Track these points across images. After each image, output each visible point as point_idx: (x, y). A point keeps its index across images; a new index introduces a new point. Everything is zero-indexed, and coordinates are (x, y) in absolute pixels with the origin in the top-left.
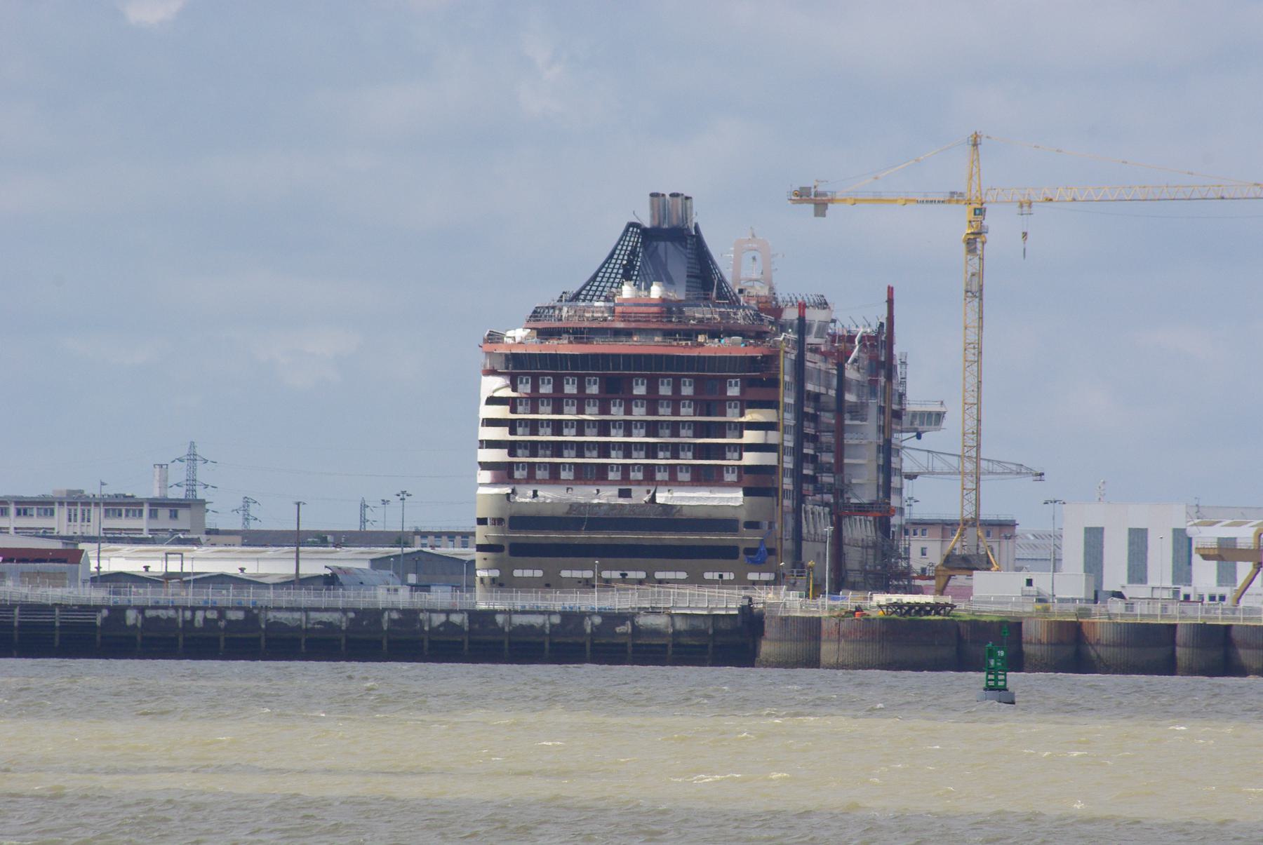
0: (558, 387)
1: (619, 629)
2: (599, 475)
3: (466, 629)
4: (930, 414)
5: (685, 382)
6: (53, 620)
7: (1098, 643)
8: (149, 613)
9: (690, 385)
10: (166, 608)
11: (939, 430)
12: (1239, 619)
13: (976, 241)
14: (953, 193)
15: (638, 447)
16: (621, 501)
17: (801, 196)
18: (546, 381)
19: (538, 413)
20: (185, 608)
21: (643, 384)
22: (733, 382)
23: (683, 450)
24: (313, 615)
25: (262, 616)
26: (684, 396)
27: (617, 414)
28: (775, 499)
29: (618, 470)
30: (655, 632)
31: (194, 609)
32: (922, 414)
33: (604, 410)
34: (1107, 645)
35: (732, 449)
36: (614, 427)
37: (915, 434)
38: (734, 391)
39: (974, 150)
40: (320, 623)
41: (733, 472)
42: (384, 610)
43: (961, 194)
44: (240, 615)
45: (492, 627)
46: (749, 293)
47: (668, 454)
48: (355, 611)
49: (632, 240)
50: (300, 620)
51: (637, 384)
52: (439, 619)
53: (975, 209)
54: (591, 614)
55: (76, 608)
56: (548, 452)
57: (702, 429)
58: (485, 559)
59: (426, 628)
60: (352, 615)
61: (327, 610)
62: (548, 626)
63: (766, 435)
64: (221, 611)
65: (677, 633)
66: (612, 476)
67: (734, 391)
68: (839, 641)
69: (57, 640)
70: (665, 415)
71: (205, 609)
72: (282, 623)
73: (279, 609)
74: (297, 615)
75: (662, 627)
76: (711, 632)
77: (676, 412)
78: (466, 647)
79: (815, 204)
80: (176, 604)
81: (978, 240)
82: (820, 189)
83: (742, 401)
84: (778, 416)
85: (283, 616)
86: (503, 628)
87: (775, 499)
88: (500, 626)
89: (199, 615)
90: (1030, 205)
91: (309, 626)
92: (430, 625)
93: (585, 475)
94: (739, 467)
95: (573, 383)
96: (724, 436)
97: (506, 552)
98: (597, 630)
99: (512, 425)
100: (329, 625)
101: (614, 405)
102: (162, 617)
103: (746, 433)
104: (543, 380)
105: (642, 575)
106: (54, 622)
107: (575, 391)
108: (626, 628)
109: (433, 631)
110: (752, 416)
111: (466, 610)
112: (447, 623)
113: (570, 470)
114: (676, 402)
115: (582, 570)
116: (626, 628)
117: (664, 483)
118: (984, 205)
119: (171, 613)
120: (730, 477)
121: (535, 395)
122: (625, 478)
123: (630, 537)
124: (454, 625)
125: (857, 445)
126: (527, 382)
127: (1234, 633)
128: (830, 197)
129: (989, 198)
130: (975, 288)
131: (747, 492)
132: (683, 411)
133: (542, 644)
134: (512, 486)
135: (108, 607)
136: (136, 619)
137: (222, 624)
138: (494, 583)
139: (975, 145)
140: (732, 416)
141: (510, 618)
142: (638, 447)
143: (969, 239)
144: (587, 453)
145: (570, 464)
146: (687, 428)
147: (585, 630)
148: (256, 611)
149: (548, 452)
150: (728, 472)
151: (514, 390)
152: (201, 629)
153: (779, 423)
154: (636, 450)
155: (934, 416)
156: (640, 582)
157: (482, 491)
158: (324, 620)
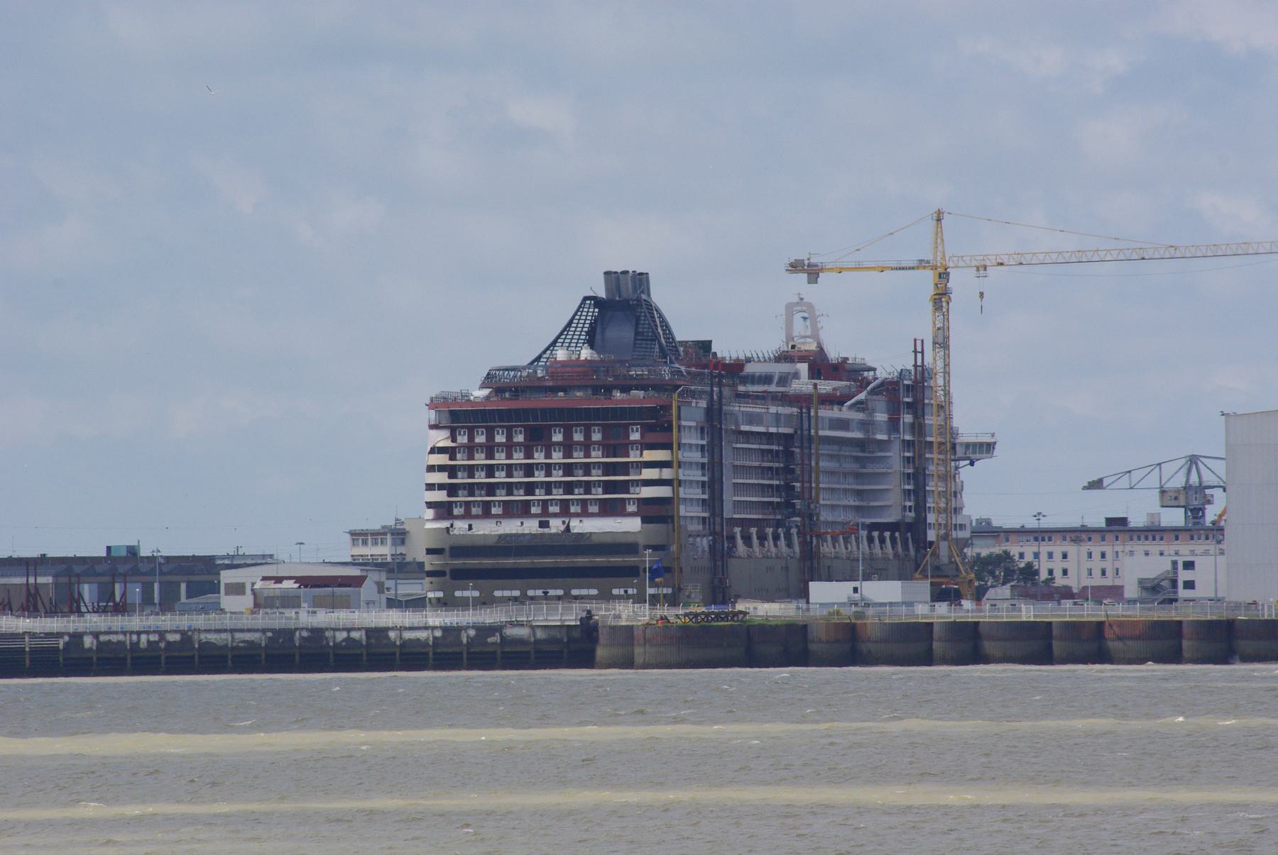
0: (490, 437)
1: (490, 640)
2: (523, 510)
3: (364, 643)
4: (981, 444)
5: (594, 429)
6: (23, 646)
7: (869, 640)
8: (102, 638)
9: (599, 432)
10: (116, 633)
11: (991, 457)
12: (1002, 617)
13: (942, 302)
14: (922, 261)
15: (557, 486)
16: (541, 530)
17: (796, 267)
18: (480, 433)
19: (474, 459)
20: (132, 633)
21: (560, 432)
22: (635, 429)
23: (594, 487)
24: (238, 636)
25: (196, 637)
26: (554, 442)
27: (539, 458)
28: (671, 525)
29: (538, 505)
30: (520, 641)
31: (139, 633)
32: (975, 445)
33: (529, 455)
34: (876, 642)
35: (635, 484)
36: (537, 469)
37: (968, 462)
38: (635, 436)
39: (938, 224)
40: (243, 642)
41: (634, 504)
42: (296, 629)
43: (928, 262)
44: (177, 637)
45: (385, 641)
46: (800, 348)
47: (582, 490)
48: (272, 630)
49: (592, 312)
50: (227, 640)
51: (555, 432)
52: (341, 636)
53: (940, 274)
54: (466, 628)
55: (42, 635)
56: (483, 492)
57: (609, 469)
58: (431, 583)
59: (331, 644)
60: (270, 634)
61: (249, 630)
62: (431, 639)
63: (661, 471)
64: (162, 634)
65: (537, 642)
66: (534, 510)
67: (635, 436)
68: (645, 645)
69: (27, 662)
70: (578, 458)
71: (147, 633)
72: (213, 643)
73: (208, 631)
74: (224, 636)
75: (525, 637)
76: (565, 640)
77: (587, 455)
78: (365, 658)
79: (808, 273)
80: (124, 630)
81: (943, 300)
82: (813, 261)
83: (641, 445)
84: (672, 455)
85: (212, 637)
86: (395, 642)
87: (671, 525)
88: (393, 640)
89: (144, 638)
90: (985, 268)
91: (235, 644)
92: (334, 642)
93: (510, 510)
94: (638, 499)
95: (503, 434)
96: (628, 474)
97: (448, 577)
98: (471, 641)
99: (452, 471)
100: (251, 644)
101: (537, 451)
102: (114, 640)
103: (644, 471)
104: (478, 432)
105: (560, 592)
106: (24, 648)
107: (504, 440)
108: (496, 639)
109: (337, 645)
110: (649, 455)
111: (363, 628)
112: (348, 639)
113: (499, 506)
114: (587, 447)
115: (511, 590)
116: (495, 639)
117: (576, 515)
118: (948, 270)
119: (121, 637)
120: (631, 508)
121: (471, 444)
122: (545, 512)
123: (548, 561)
124: (354, 640)
125: (883, 473)
126: (464, 434)
127: (981, 628)
128: (820, 267)
129: (951, 264)
130: (940, 340)
131: (645, 520)
132: (593, 454)
133: (427, 653)
134: (451, 522)
135: (69, 634)
136: (92, 643)
137: (162, 645)
138: (439, 602)
139: (939, 220)
140: (634, 457)
141: (401, 634)
142: (557, 486)
143: (935, 299)
144: (515, 492)
145: (499, 501)
146: (597, 468)
147: (462, 641)
148: (190, 633)
149: (483, 492)
150: (629, 504)
151: (454, 440)
152: (146, 650)
153: (673, 461)
154: (555, 487)
155: (985, 446)
156: (559, 598)
157: (429, 526)
158: (247, 639)
